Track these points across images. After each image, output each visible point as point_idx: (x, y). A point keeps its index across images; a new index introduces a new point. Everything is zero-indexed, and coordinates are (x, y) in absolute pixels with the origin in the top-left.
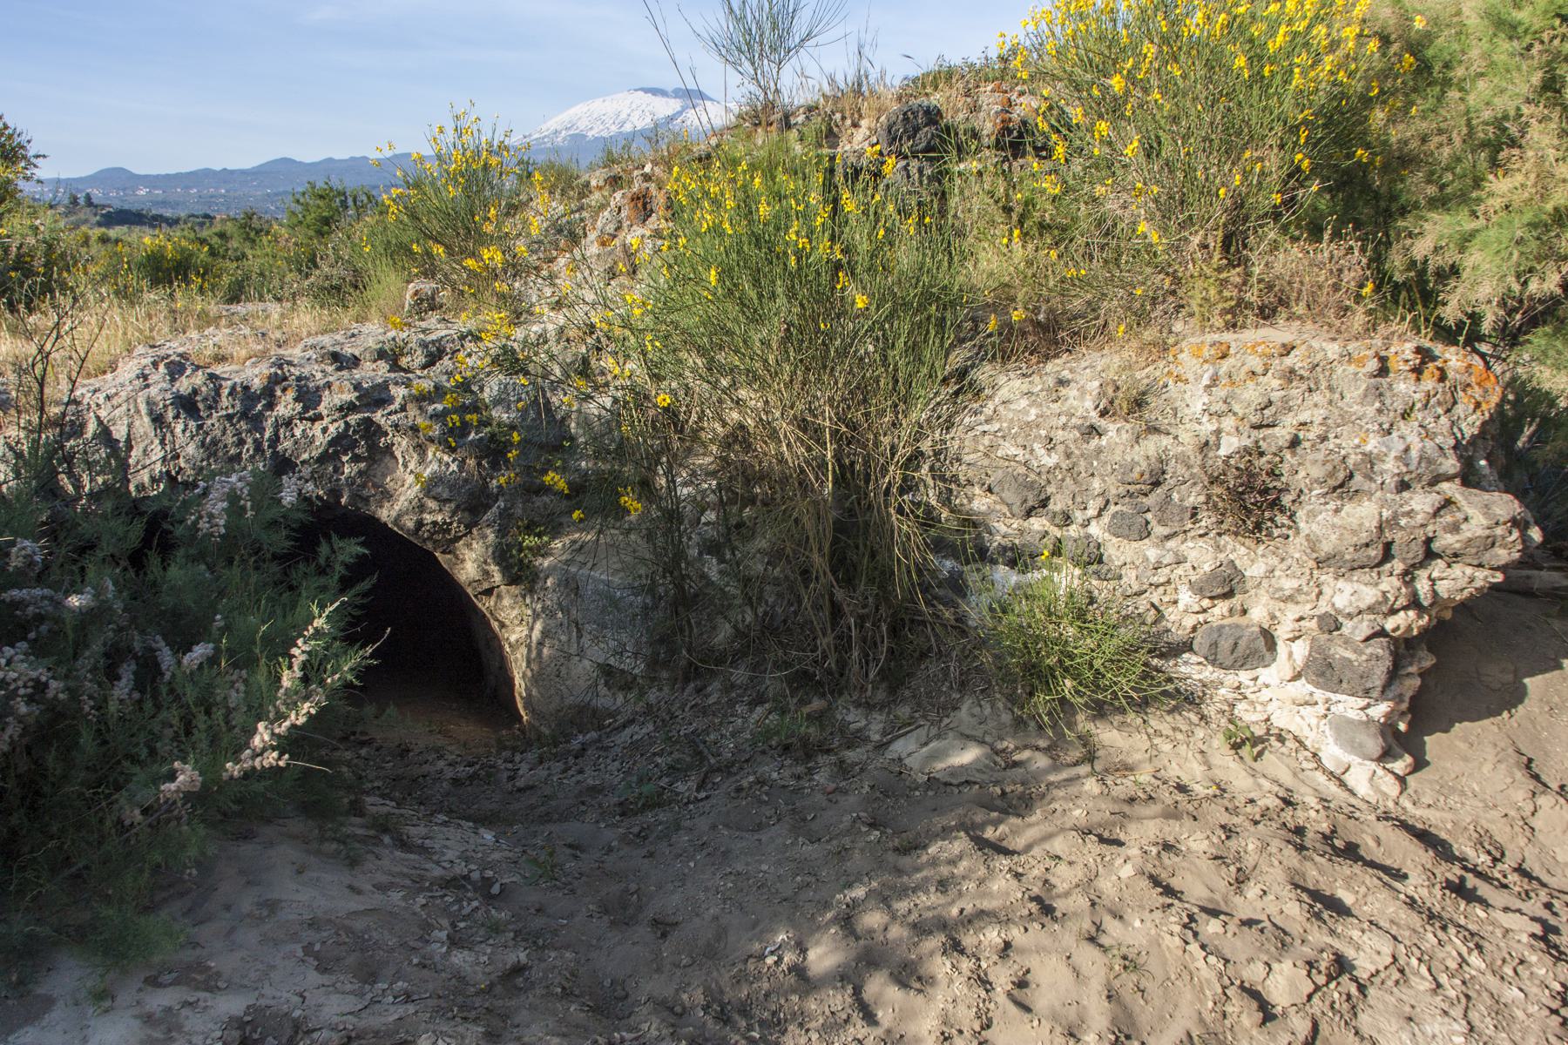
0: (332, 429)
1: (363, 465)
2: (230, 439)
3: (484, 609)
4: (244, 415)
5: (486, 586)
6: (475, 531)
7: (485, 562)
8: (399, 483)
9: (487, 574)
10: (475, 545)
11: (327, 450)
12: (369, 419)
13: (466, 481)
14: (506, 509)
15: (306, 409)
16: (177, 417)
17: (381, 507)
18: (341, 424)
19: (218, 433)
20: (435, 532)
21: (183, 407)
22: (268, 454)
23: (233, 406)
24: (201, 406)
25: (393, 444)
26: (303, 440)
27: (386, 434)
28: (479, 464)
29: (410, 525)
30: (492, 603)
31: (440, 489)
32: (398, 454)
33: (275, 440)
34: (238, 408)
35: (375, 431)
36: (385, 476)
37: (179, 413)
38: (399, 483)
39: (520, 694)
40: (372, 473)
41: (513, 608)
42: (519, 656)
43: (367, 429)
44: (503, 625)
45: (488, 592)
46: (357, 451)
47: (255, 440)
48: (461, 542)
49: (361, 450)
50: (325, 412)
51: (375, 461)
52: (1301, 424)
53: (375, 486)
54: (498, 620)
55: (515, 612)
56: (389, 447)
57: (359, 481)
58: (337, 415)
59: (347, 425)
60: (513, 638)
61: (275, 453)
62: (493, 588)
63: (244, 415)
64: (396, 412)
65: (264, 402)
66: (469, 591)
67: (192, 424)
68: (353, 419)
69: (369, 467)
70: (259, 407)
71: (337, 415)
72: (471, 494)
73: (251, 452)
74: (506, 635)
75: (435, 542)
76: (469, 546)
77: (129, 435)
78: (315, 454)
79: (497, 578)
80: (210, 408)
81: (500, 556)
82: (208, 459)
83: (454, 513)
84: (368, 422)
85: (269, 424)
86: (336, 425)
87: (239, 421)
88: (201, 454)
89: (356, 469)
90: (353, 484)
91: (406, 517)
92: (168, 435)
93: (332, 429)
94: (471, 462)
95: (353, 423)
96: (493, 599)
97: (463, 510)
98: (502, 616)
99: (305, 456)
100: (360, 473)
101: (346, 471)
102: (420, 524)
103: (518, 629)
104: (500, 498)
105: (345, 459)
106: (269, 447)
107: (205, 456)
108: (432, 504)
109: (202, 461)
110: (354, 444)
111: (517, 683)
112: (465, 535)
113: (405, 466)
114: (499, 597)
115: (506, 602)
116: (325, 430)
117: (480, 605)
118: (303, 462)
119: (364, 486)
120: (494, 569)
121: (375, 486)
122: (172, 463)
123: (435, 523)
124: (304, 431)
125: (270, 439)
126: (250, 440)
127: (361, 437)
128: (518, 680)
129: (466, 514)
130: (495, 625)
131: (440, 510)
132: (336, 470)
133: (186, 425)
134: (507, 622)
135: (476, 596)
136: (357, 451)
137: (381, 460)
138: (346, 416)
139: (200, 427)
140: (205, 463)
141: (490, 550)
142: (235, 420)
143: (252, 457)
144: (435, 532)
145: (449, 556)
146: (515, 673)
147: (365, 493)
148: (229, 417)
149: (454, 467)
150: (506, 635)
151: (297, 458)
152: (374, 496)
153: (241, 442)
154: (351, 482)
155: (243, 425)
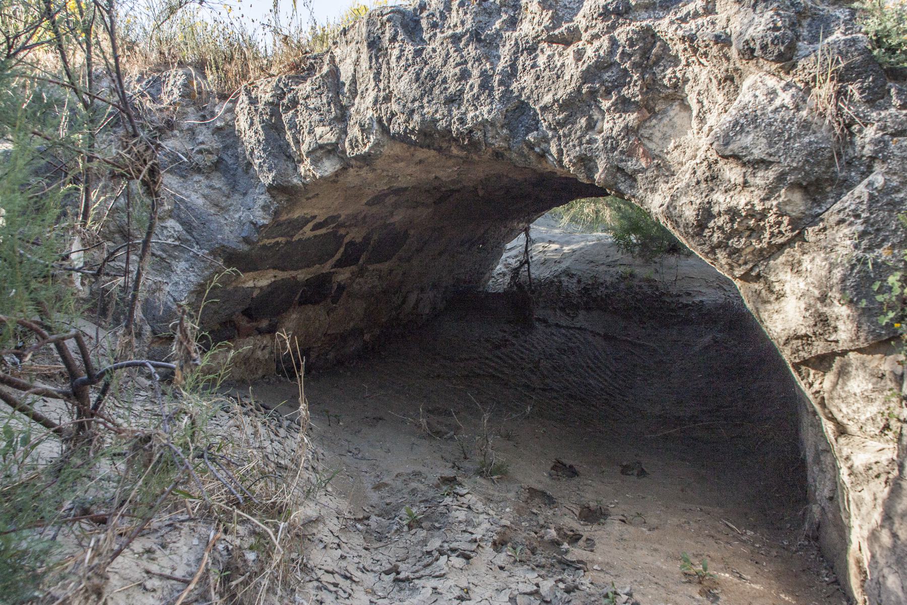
0: (590, 52)
1: (632, 118)
2: (451, 71)
3: (809, 393)
4: (476, 36)
5: (819, 348)
6: (810, 234)
7: (823, 298)
8: (689, 152)
9: (823, 321)
10: (806, 264)
11: (579, 90)
12: (648, 29)
13: (806, 126)
14: (887, 190)
15: (556, 21)
16: (393, 39)
17: (653, 190)
18: (605, 41)
19: (439, 61)
20: (734, 233)
21: (404, 26)
22: (497, 94)
23: (463, 23)
24: (424, 24)
25: (686, 81)
26: (547, 73)
27: (676, 61)
28: (841, 94)
29: (690, 214)
30: (827, 385)
31: (748, 140)
32: (692, 100)
33: (512, 73)
34: (468, 25)
35: (659, 58)
36: (665, 138)
37: (397, 33)
38: (689, 152)
39: (858, 562)
40: (645, 132)
41: (869, 400)
42: (867, 496)
43: (645, 53)
44: (842, 431)
45: (822, 362)
46: (625, 92)
47: (483, 73)
48: (782, 259)
49: (632, 91)
50: (583, 24)
51: (653, 113)
52: (359, 432)
53: (647, 154)
54: (832, 419)
55: (873, 409)
56: (678, 86)
57: (623, 144)
58: (600, 25)
59: (614, 42)
60: (860, 460)
61: (507, 92)
62: (834, 354)
63: (476, 36)
64: (696, 15)
65: (505, 17)
66: (786, 354)
67: (410, 48)
68: (623, 33)
69: (642, 123)
70: (497, 25)
71: (600, 25)
72: (813, 154)
73: (475, 90)
74: (846, 451)
75: (734, 253)
76: (795, 267)
77: (354, 76)
78: (562, 94)
79: (844, 333)
80: (434, 26)
81: (857, 287)
82: (422, 97)
83: (771, 191)
84: (649, 36)
85: (505, 52)
86: (596, 43)
87: (467, 45)
88: (414, 91)
89: (621, 123)
90: (614, 149)
91: (684, 199)
92: (384, 66)
93: (590, 52)
94: (825, 90)
95: (622, 39)
96: (830, 378)
97: (796, 186)
98: (842, 411)
99: (547, 99)
100: (628, 130)
101: (606, 126)
102: (706, 214)
103: (875, 445)
104: (878, 167)
105: (605, 104)
106: (501, 83)
107: (418, 94)
108: (732, 173)
109: (413, 101)
110: (623, 79)
111: (853, 547)
112: (789, 243)
113: (702, 120)
114: (843, 373)
115: (858, 384)
116: (579, 55)
117: (802, 385)
118: (544, 109)
119: (630, 153)
120: (840, 311)
121: (647, 154)
122: (384, 107)
123: (733, 213)
124: (550, 57)
125: (502, 72)
126: (476, 73)
127: (635, 65)
128: (858, 536)
129: (797, 197)
130: (829, 428)
131: (745, 184)
132: (591, 126)
133: (402, 51)
134: (852, 428)
135: (797, 366)
136: (625, 92)
137: (665, 112)
138: (613, 27)
139: (418, 53)
140: (417, 104)
141: (838, 274)
142: (461, 45)
143: (476, 98)
144: (734, 233)
145: (756, 286)
146: (855, 522)
147: (630, 165)
148: (456, 39)
149: (785, 98)
150: (846, 451)
151: (536, 101)
152: (644, 170)
153: (464, 75)
154: (612, 145)
155: (472, 51)
